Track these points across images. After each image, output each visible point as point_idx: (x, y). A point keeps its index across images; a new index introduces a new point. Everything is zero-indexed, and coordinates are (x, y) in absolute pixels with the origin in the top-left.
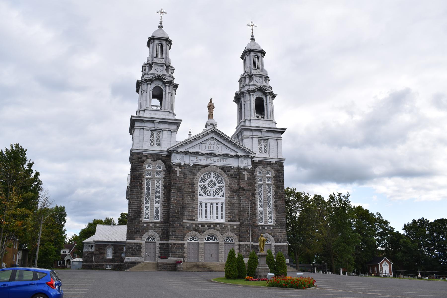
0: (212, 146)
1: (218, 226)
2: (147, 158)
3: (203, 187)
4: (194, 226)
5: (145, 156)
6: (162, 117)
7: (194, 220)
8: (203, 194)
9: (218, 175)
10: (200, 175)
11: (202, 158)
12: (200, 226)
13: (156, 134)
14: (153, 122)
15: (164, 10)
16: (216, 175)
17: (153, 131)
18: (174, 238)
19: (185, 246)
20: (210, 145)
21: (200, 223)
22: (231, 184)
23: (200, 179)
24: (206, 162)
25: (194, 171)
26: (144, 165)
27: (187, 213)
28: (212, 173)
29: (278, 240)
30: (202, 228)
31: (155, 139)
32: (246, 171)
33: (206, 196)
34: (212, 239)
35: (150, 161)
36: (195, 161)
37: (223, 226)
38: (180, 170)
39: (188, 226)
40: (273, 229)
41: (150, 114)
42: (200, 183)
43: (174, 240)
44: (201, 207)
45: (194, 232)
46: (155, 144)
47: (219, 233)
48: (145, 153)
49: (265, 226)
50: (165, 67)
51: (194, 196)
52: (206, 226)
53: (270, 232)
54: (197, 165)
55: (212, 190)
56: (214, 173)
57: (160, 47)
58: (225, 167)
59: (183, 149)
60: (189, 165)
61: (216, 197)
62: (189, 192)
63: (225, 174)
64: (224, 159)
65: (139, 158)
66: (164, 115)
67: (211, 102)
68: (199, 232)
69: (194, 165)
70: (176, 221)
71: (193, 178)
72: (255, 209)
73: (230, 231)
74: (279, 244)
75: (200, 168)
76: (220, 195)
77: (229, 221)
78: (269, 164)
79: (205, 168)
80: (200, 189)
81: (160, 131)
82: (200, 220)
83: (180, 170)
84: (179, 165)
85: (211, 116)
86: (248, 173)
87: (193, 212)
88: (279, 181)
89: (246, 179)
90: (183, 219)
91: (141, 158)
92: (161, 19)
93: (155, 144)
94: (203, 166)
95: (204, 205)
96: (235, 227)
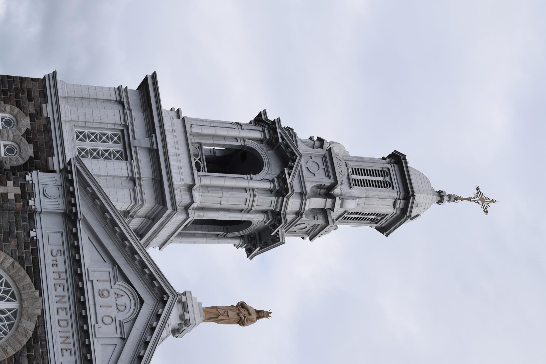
0: (111, 300)
2: (33, 118)
5: (39, 112)
6: (171, 150)
9: (10, 326)
11: (61, 268)
13: (112, 147)
14: (150, 130)
15: (491, 208)
16: (8, 319)
17: (124, 135)
20: (113, 295)
24: (51, 282)
25: (13, 243)
26: (8, 107)
28: (13, 305)
31: (100, 146)
35: (26, 123)
36: (48, 248)
38: (11, 196)
41: (173, 131)
46: (82, 145)
48: (48, 110)
50: (328, 182)
54: (35, 252)
56: (15, 314)
57: (381, 179)
58: (45, 346)
59: (83, 208)
60: (32, 226)
63: (19, 347)
64: (72, 343)
65: (29, 94)
66: (180, 169)
67: (261, 314)
69: (35, 243)
75: (29, 263)
79: (28, 280)
81: (126, 154)
83: (11, 196)
84: (26, 193)
85: (215, 315)
91: (30, 99)
92: (462, 199)
93: (82, 145)
94: (34, 272)
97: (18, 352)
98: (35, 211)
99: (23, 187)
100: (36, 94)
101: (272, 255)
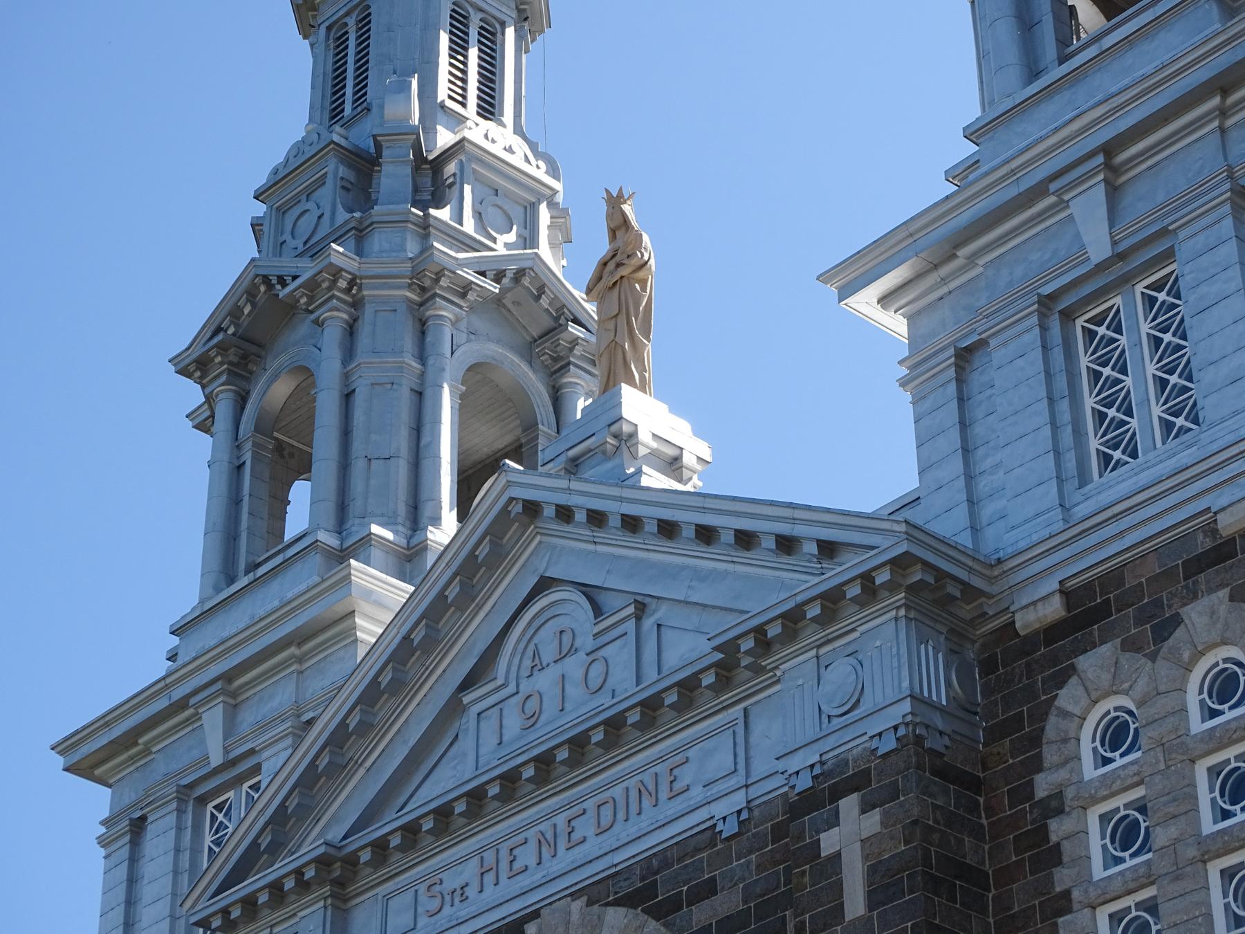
86: (872, 822)
89: (855, 904)
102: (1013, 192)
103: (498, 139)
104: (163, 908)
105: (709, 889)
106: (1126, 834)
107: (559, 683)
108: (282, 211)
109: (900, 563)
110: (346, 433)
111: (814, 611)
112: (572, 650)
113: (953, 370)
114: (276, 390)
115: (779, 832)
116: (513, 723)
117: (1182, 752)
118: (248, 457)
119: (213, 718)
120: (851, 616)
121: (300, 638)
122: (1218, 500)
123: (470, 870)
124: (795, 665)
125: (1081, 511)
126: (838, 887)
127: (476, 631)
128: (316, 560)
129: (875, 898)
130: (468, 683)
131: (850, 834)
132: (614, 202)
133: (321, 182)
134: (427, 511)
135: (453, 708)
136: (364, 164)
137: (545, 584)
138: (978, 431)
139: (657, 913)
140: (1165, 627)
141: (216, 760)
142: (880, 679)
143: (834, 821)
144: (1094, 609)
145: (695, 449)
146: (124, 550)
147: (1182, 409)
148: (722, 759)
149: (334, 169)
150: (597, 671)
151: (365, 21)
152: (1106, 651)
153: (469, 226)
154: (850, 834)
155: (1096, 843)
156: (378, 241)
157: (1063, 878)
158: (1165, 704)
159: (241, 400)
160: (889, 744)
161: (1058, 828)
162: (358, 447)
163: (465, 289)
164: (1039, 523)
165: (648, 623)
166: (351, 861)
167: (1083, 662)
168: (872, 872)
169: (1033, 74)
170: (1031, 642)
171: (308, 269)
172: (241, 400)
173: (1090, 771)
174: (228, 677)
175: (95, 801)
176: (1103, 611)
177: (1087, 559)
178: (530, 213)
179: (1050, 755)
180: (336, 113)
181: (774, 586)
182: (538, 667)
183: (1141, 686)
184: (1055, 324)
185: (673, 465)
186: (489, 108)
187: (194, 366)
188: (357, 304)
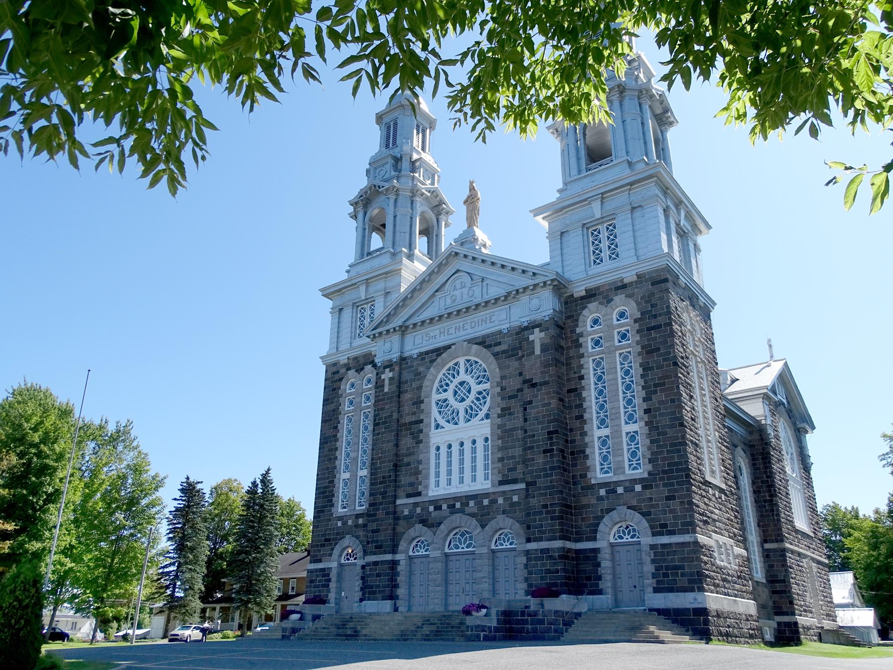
1: (472, 503)
2: (349, 369)
3: (443, 404)
4: (419, 510)
7: (419, 494)
8: (442, 422)
10: (437, 374)
12: (431, 508)
18: (376, 547)
19: (399, 568)
21: (431, 502)
22: (503, 378)
23: (436, 385)
24: (447, 337)
25: (421, 369)
27: (404, 479)
29: (664, 526)
30: (437, 512)
32: (537, 330)
33: (450, 426)
34: (508, 540)
35: (352, 373)
37: (486, 502)
38: (391, 374)
39: (406, 512)
40: (645, 487)
42: (435, 397)
43: (375, 554)
44: (438, 457)
45: (419, 526)
47: (474, 522)
49: (618, 483)
51: (421, 431)
52: (444, 507)
53: (634, 503)
54: (427, 353)
55: (461, 407)
58: (488, 336)
59: (397, 322)
61: (475, 421)
62: (411, 423)
65: (334, 373)
68: (431, 526)
69: (421, 354)
70: (381, 504)
71: (420, 388)
72: (584, 434)
73: (504, 512)
74: (665, 540)
76: (482, 414)
77: (501, 483)
78: (621, 287)
80: (435, 410)
82: (434, 492)
83: (391, 374)
86: (543, 334)
87: (417, 472)
88: (654, 328)
89: (538, 351)
90: (395, 497)
91: (338, 372)
95: (444, 450)
96: (515, 499)
97: (372, 464)
98: (401, 357)
99: (385, 367)
100: (334, 369)
101: (374, 119)
102: (579, 199)
103: (427, 157)
104: (349, 330)
105: (499, 344)
106: (597, 343)
107: (461, 293)
108: (375, 169)
109: (552, 280)
110: (395, 225)
111: (531, 288)
112: (464, 287)
113: (559, 236)
114: (374, 211)
115: (517, 334)
116: (449, 301)
117: (611, 327)
118: (367, 227)
119: (363, 288)
120: (538, 289)
121: (386, 273)
122: (624, 276)
123: (437, 332)
124: (524, 298)
125: (590, 273)
126: (534, 348)
127: (441, 279)
128: (388, 255)
129: (542, 351)
130: (436, 291)
131: (537, 337)
132: (471, 183)
133: (387, 163)
134: (413, 246)
135: (433, 295)
136: (397, 160)
137: (457, 271)
138: (565, 251)
139: (486, 347)
140: (610, 301)
141: (363, 298)
142: (544, 305)
143: (533, 333)
144: (591, 295)
145: (489, 243)
146: (335, 246)
147: (614, 255)
148: (504, 316)
149: (391, 161)
150: (471, 292)
151: (396, 124)
152: (596, 304)
153: (421, 178)
154: (537, 337)
155: (590, 344)
156: (402, 180)
157: (582, 351)
158: (608, 317)
159: (365, 214)
160: (547, 318)
161: (581, 340)
162: (398, 228)
163: (423, 194)
164: (581, 276)
165: (484, 283)
166: (407, 327)
167: (589, 305)
168: (542, 345)
169: (580, 172)
170: (576, 300)
171: (387, 185)
172: (365, 214)
173: (589, 329)
174: (367, 280)
175: (329, 303)
176: (594, 295)
177: (592, 284)
178: (433, 176)
179: (580, 324)
180: (387, 146)
181: (521, 281)
182: (455, 289)
183: (603, 312)
184: (585, 229)
185: (484, 246)
186: (423, 149)
187: (354, 204)
188: (397, 195)
